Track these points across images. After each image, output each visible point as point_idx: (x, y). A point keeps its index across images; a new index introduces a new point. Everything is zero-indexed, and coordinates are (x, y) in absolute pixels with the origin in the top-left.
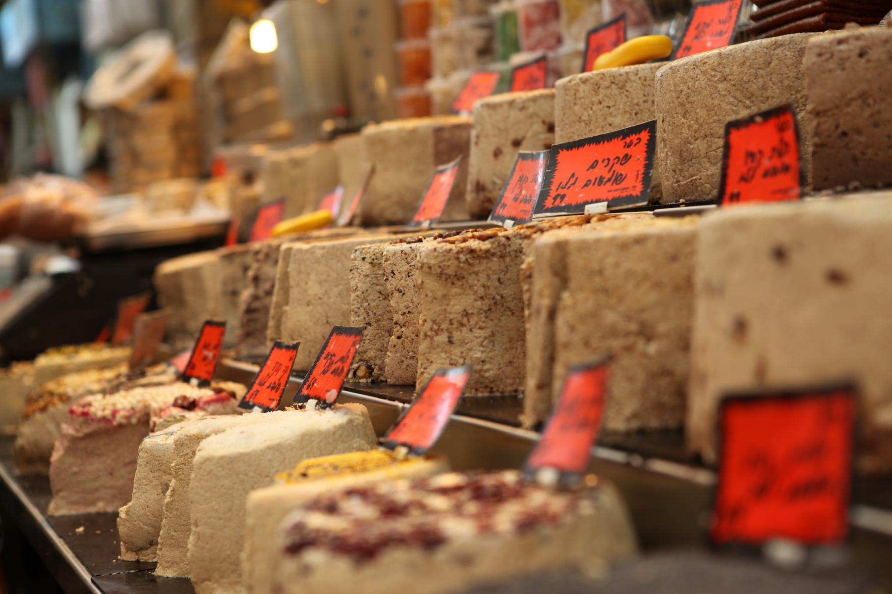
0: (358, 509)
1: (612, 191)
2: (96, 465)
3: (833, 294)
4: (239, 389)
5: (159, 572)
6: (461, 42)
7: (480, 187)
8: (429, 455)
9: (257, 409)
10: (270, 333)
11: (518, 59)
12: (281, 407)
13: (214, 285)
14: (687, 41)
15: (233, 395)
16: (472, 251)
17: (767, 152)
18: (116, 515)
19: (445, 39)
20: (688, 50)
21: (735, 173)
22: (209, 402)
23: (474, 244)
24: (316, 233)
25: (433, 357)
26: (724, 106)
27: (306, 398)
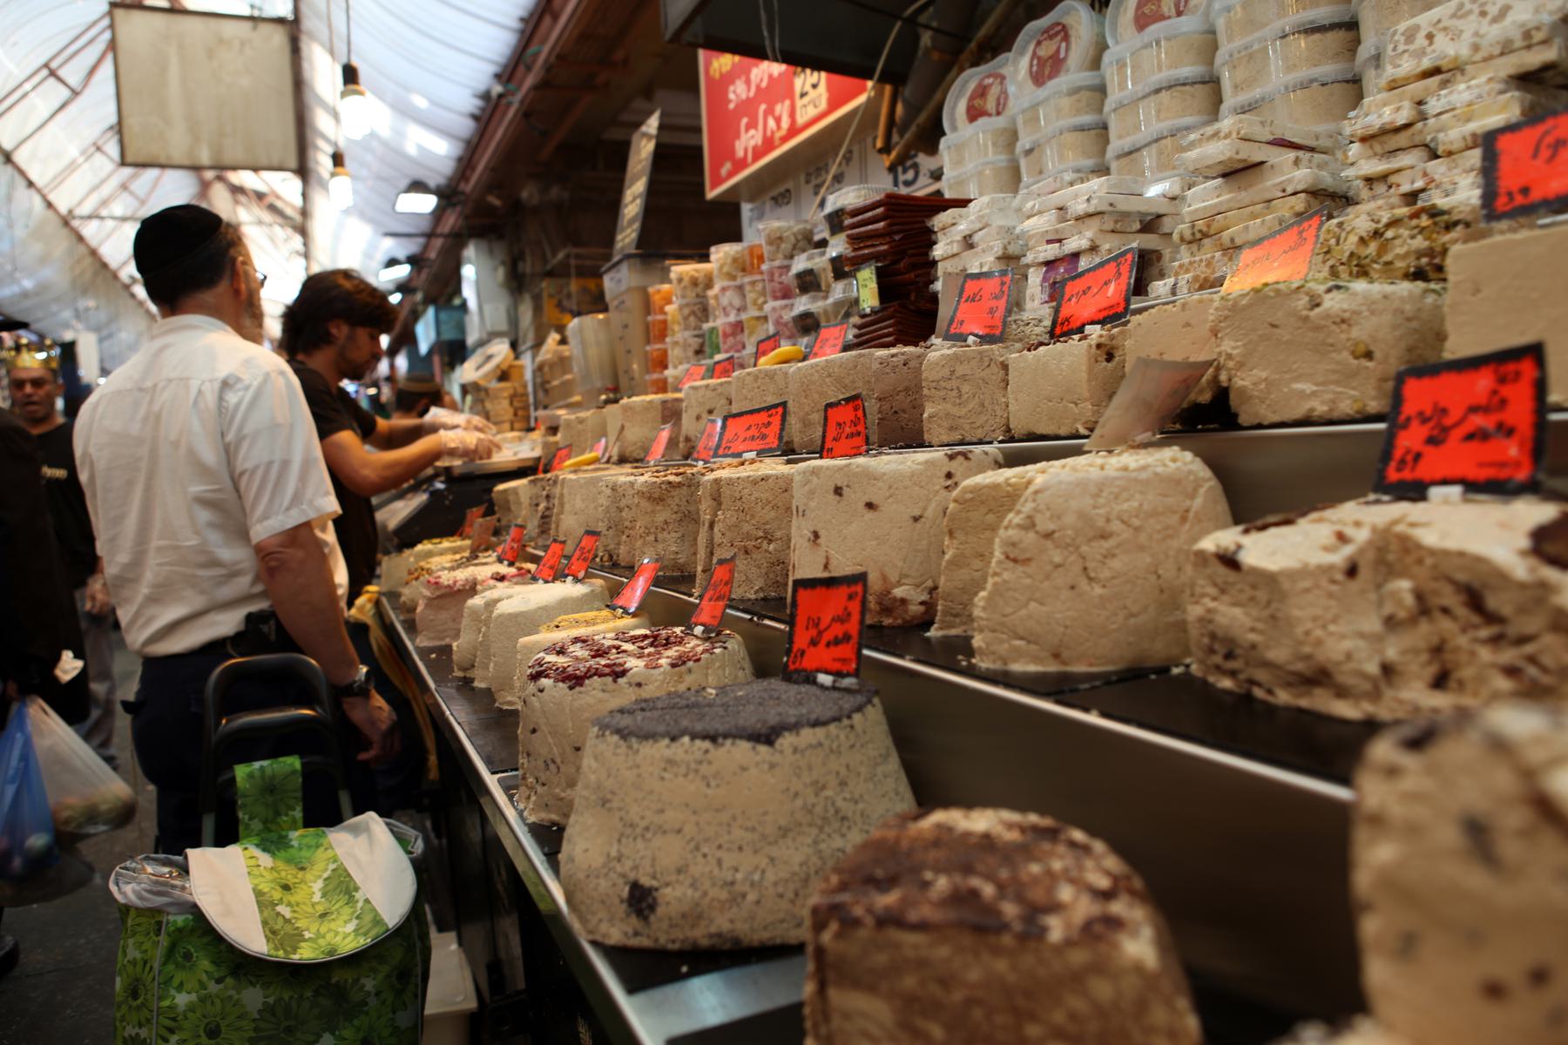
0: (578, 651)
1: (760, 445)
2: (444, 615)
3: (869, 515)
4: (532, 567)
5: (476, 684)
6: (686, 346)
7: (688, 439)
8: (634, 615)
9: (541, 581)
10: (552, 532)
11: (718, 357)
12: (553, 581)
13: (525, 499)
14: (815, 349)
15: (529, 571)
16: (670, 483)
17: (848, 423)
18: (450, 647)
19: (676, 343)
20: (816, 355)
21: (829, 437)
22: (513, 576)
23: (671, 478)
24: (586, 468)
25: (646, 550)
26: (830, 392)
27: (566, 576)
